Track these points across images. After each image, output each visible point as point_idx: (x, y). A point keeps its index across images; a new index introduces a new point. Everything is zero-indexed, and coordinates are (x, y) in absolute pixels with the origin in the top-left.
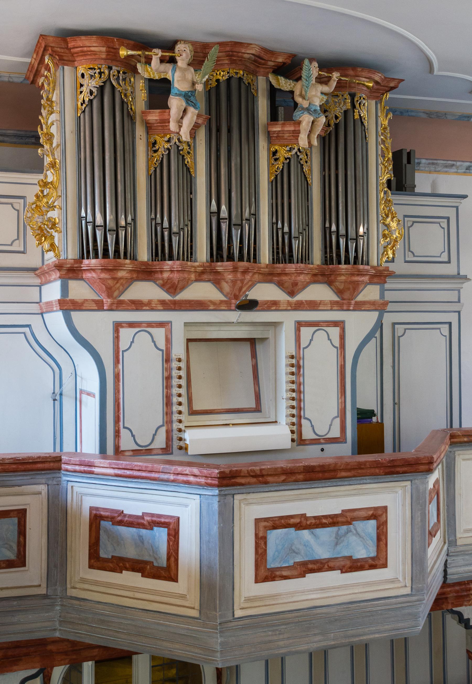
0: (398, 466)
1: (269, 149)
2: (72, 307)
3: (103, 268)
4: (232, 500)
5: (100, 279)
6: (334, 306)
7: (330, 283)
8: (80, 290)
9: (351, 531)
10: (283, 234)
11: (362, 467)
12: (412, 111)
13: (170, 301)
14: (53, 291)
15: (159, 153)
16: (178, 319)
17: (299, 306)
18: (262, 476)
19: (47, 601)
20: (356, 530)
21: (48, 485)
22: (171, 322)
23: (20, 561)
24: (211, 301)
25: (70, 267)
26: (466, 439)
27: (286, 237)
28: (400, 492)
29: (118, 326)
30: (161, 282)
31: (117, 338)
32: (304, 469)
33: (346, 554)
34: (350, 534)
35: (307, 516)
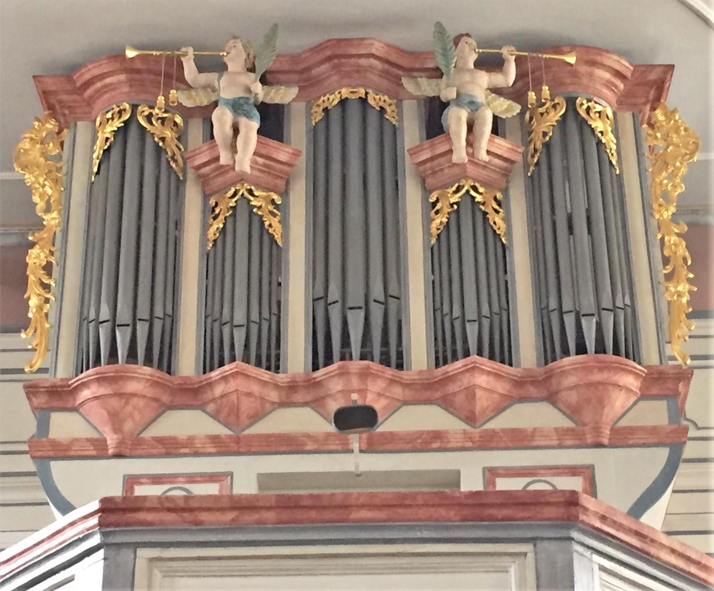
0: (492, 505)
2: (51, 453)
4: (132, 556)
6: (564, 439)
7: (552, 398)
11: (407, 502)
13: (230, 437)
15: (222, 217)
18: (191, 510)
22: (231, 474)
24: (308, 436)
28: (512, 570)
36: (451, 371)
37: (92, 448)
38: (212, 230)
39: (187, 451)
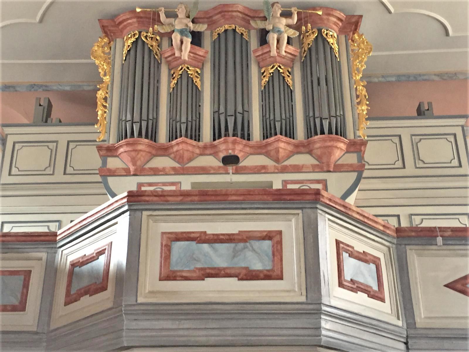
1: (259, 71)
2: (108, 174)
3: (126, 143)
6: (315, 169)
7: (310, 153)
9: (247, 247)
11: (252, 193)
12: (424, 75)
17: (284, 170)
18: (164, 196)
19: (36, 337)
20: (252, 247)
21: (48, 253)
22: (180, 183)
23: (21, 307)
24: (211, 167)
26: (413, 234)
28: (293, 220)
32: (198, 192)
33: (243, 265)
34: (246, 250)
35: (207, 233)
39: (163, 173)
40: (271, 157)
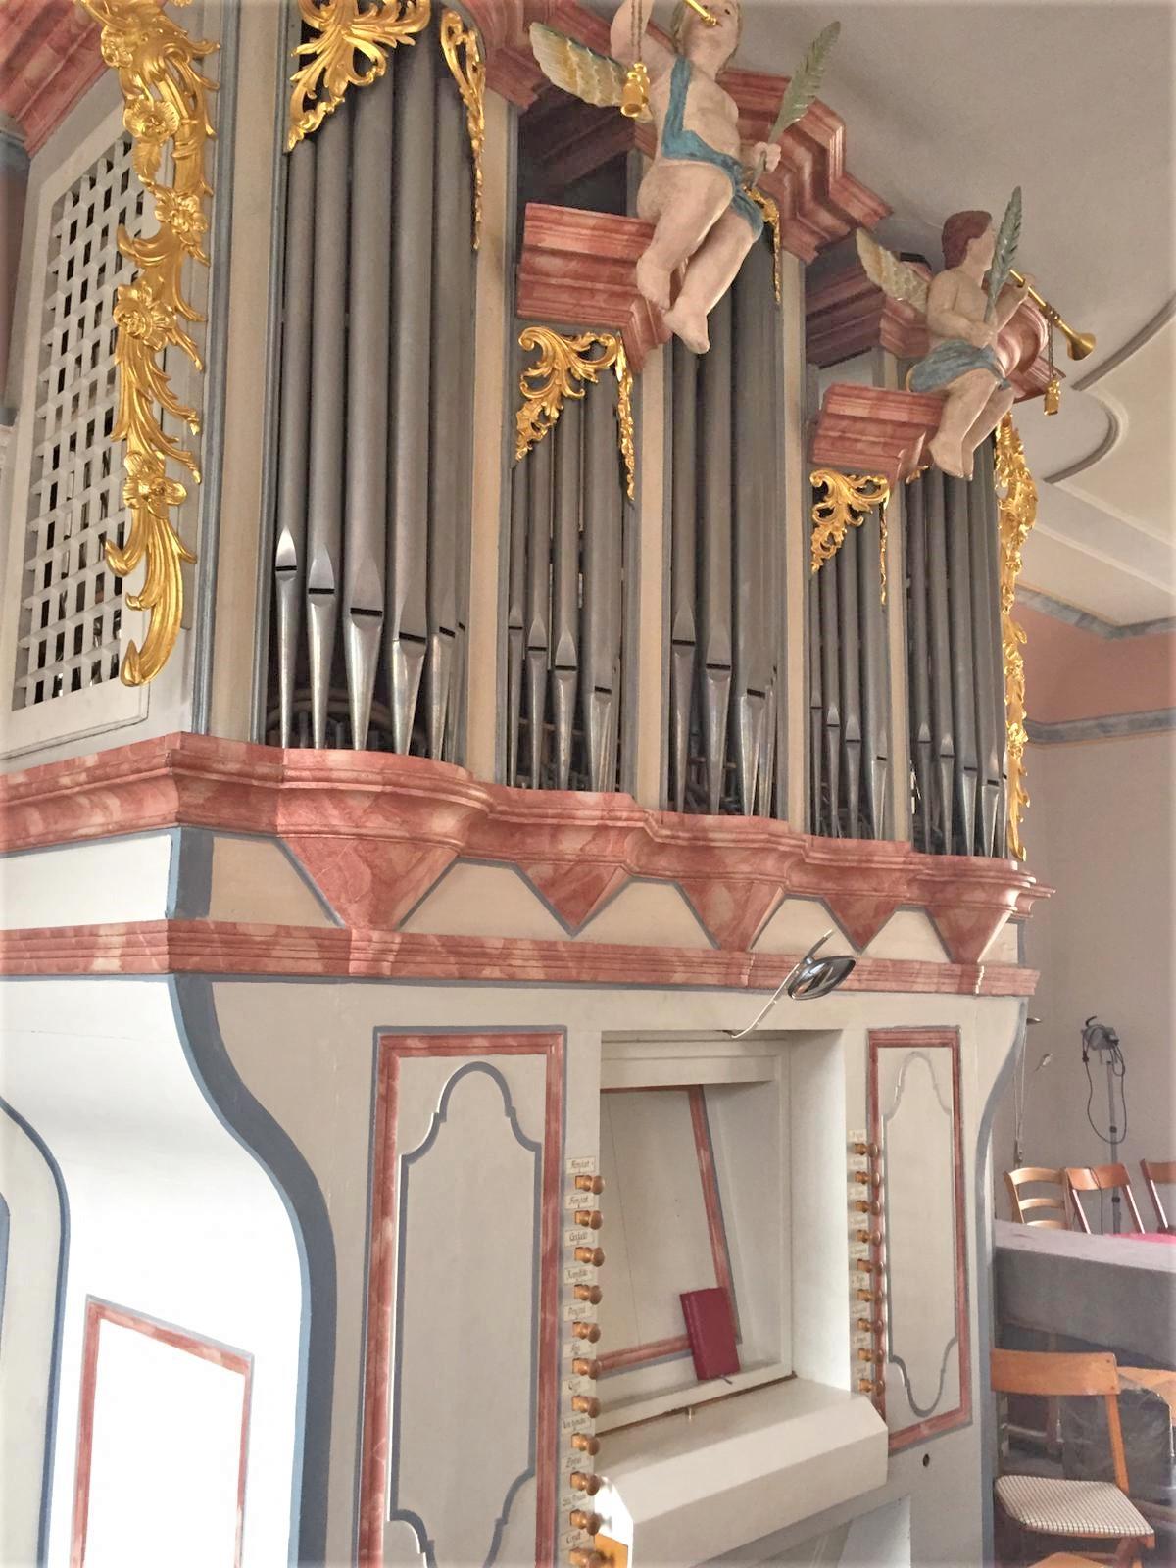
2: (221, 963)
3: (389, 789)
5: (360, 837)
8: (255, 884)
10: (843, 743)
14: (126, 880)
16: (586, 1015)
22: (563, 1030)
25: (240, 774)
27: (852, 755)
29: (391, 1045)
30: (545, 870)
31: (384, 1102)
36: (878, 863)
37: (316, 955)
38: (529, 414)
39: (496, 973)
40: (844, 916)
